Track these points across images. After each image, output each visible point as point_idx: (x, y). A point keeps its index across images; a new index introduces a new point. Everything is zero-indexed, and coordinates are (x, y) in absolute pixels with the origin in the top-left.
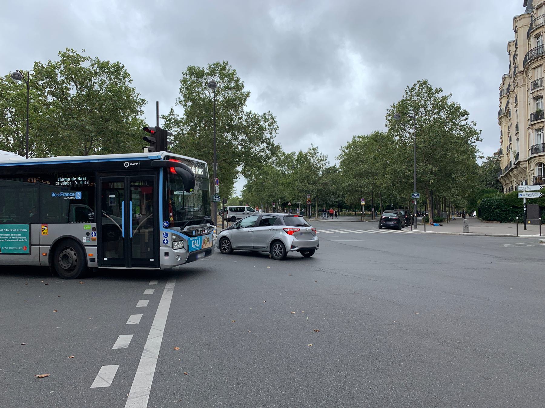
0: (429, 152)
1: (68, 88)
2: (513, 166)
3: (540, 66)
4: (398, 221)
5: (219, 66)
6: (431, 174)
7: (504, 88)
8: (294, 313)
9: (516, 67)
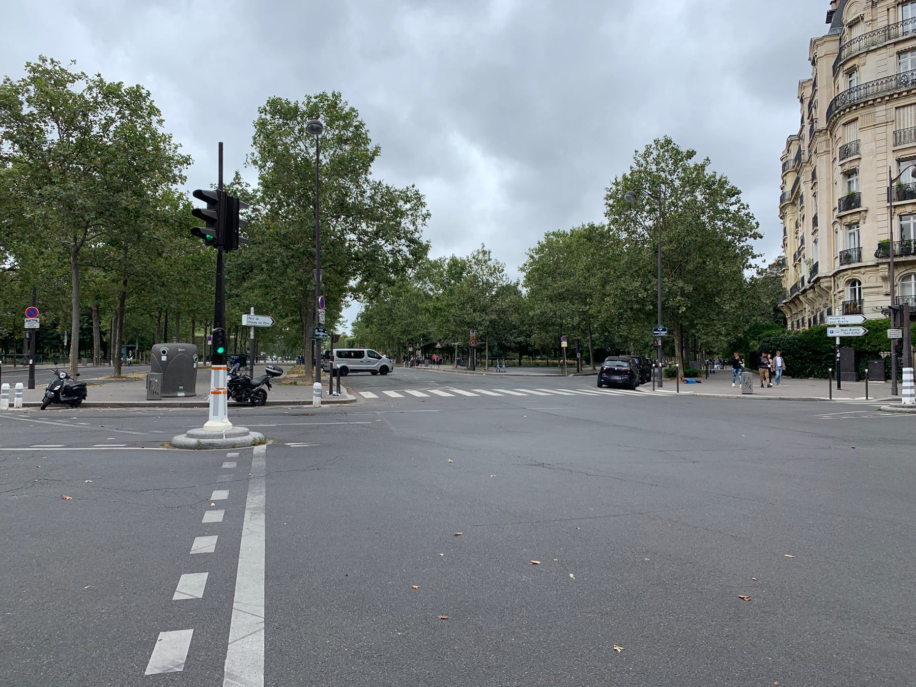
0: (677, 258)
1: (42, 130)
2: (807, 285)
3: (854, 121)
4: (631, 374)
5: (326, 100)
6: (682, 296)
7: (789, 158)
8: (538, 562)
9: (812, 121)
